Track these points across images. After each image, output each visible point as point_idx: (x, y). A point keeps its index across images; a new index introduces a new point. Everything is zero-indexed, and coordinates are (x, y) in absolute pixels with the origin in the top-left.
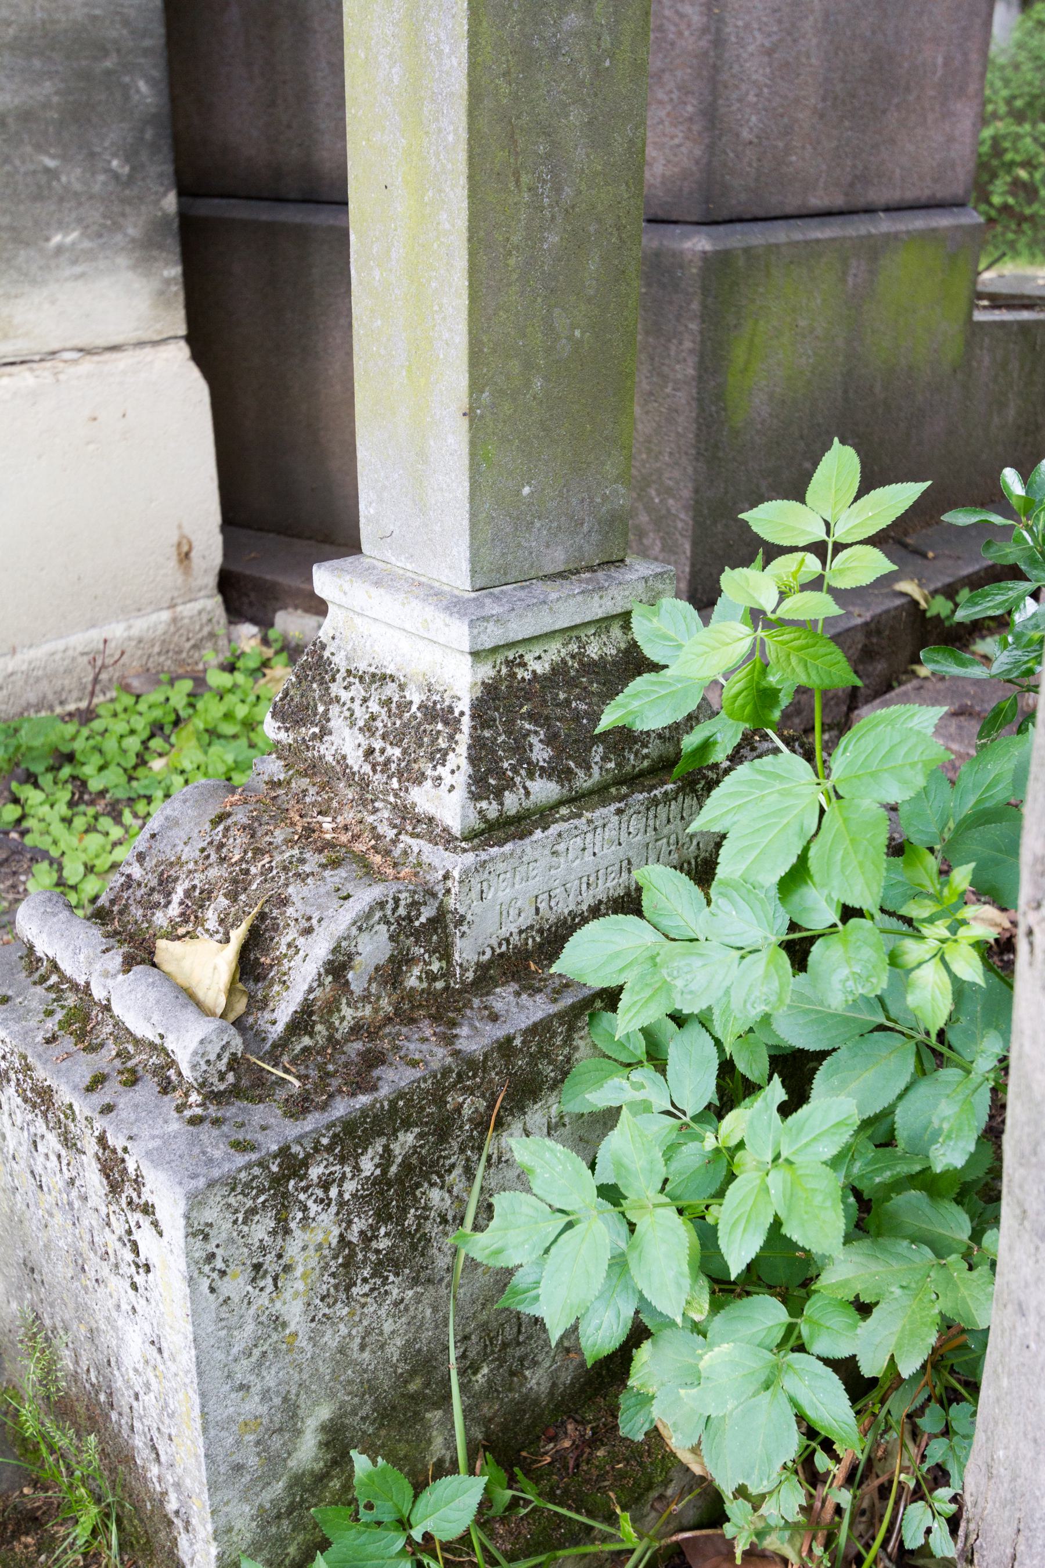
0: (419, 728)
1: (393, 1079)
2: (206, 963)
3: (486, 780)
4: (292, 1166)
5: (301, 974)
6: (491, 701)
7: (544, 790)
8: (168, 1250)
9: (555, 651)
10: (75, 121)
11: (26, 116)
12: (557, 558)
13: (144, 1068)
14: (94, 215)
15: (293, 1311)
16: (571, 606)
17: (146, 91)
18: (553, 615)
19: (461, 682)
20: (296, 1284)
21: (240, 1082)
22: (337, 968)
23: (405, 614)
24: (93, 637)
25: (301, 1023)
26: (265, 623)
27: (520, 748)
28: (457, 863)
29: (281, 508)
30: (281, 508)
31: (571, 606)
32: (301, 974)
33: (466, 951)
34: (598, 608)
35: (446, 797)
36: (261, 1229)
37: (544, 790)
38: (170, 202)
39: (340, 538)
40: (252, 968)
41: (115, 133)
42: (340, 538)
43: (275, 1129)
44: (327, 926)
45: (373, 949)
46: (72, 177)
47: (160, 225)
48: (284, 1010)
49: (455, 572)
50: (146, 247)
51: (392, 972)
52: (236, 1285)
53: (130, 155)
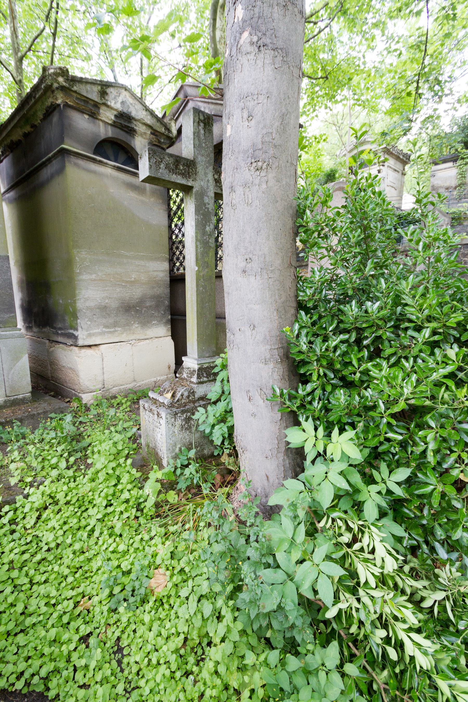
0: (192, 373)
1: (187, 407)
2: (169, 395)
3: (199, 377)
4: (176, 414)
5: (178, 396)
6: (199, 369)
7: (205, 379)
8: (163, 421)
9: (207, 365)
10: (157, 307)
11: (150, 306)
12: (207, 355)
13: (162, 405)
14: (159, 319)
15: (176, 431)
16: (209, 360)
17: (167, 303)
18: (206, 361)
19: (196, 367)
20: (176, 428)
21: (171, 405)
22: (182, 395)
23: (191, 362)
24: (155, 379)
25: (178, 401)
26: (196, 460)
27: (203, 374)
28: (195, 386)
29: (180, 351)
30: (180, 351)
31: (209, 360)
32: (178, 396)
33: (197, 396)
34: (212, 360)
35: (194, 379)
36: (173, 420)
37: (205, 379)
38: (170, 317)
39: (186, 355)
40: (173, 396)
41: (162, 308)
42: (186, 355)
43: (174, 410)
44: (181, 391)
45: (186, 394)
46: (156, 314)
47: (168, 320)
48: (176, 399)
49: (196, 357)
50: (166, 323)
51: (188, 397)
52: (170, 426)
53: (164, 311)
